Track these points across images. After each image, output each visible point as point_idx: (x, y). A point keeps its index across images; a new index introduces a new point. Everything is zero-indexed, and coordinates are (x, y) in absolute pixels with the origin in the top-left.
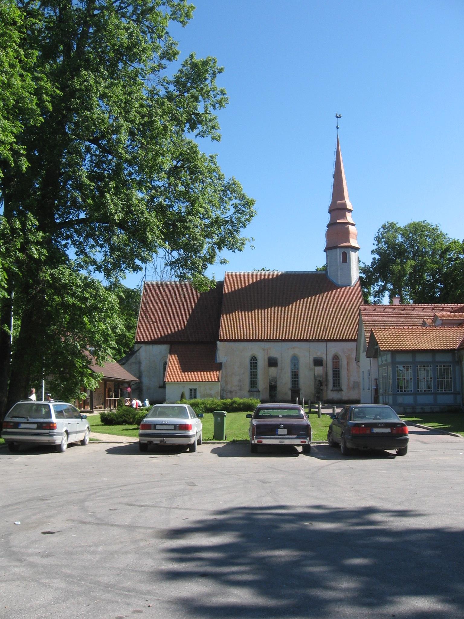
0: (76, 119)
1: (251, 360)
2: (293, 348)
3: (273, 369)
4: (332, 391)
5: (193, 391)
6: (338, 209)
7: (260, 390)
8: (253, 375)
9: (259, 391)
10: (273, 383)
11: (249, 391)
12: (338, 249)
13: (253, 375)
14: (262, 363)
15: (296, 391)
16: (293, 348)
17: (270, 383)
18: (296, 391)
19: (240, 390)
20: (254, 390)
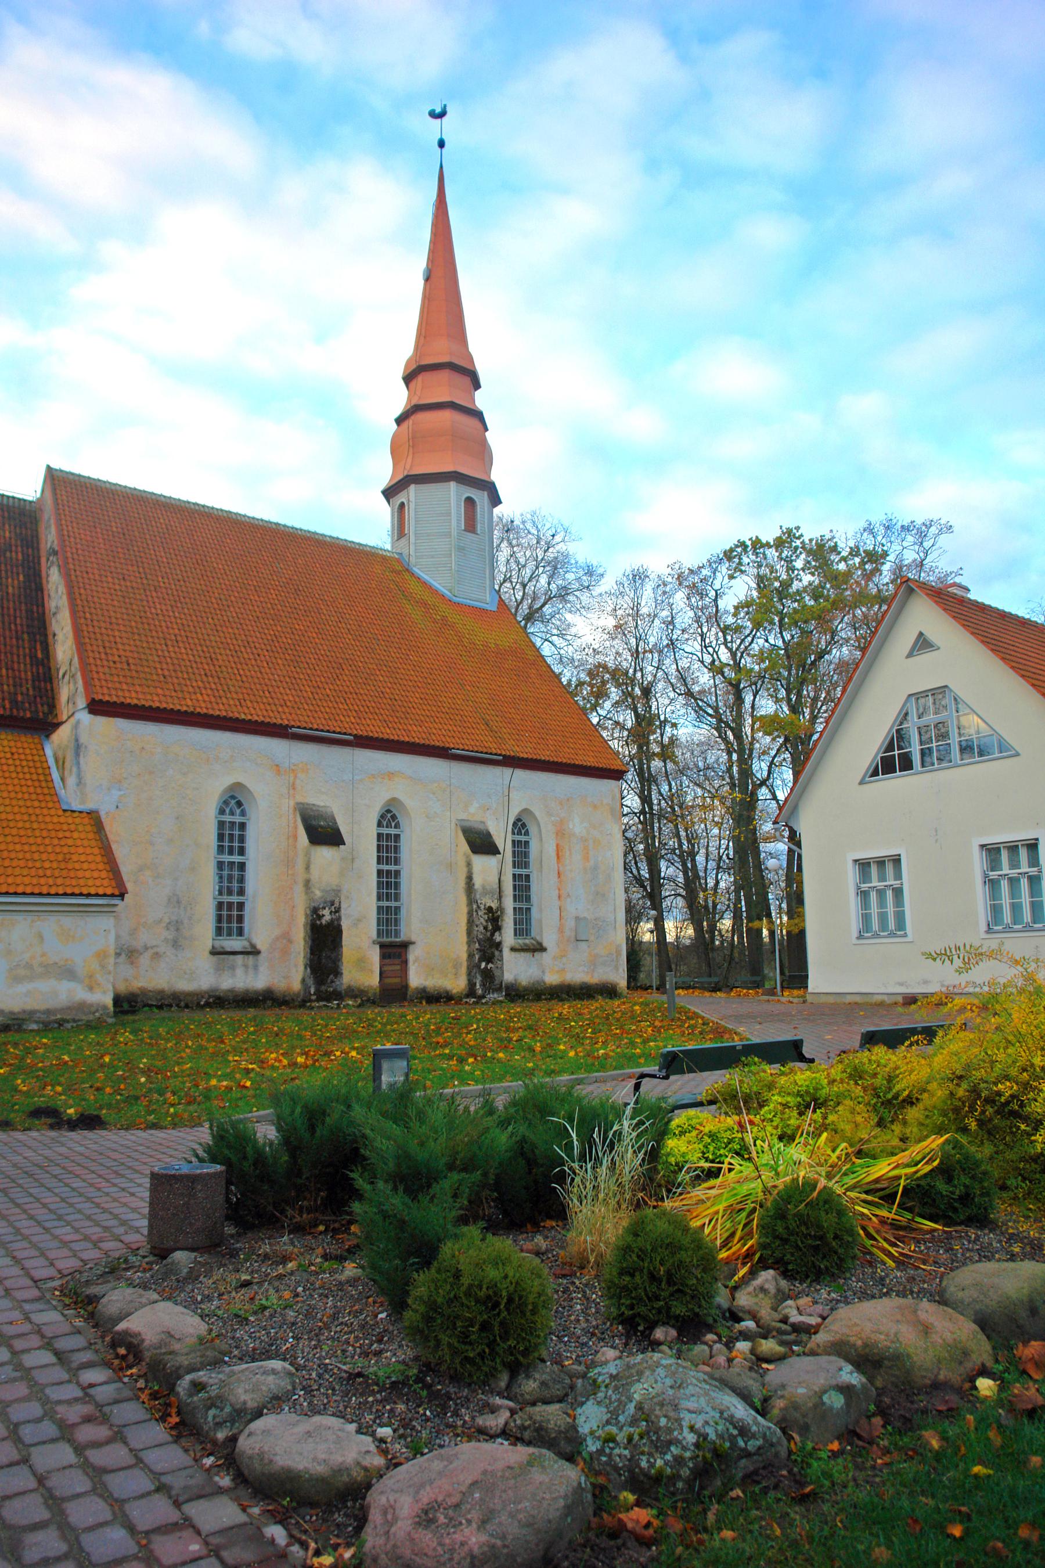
0: (905, 1503)
1: (222, 812)
2: (391, 775)
3: (325, 854)
4: (513, 949)
5: (892, 924)
6: (441, 167)
7: (259, 946)
8: (232, 877)
9: (254, 952)
10: (327, 916)
11: (214, 952)
12: (453, 485)
13: (232, 877)
14: (271, 832)
15: (802, 997)
16: (391, 775)
17: (315, 912)
18: (802, 997)
19: (176, 944)
20: (235, 944)
